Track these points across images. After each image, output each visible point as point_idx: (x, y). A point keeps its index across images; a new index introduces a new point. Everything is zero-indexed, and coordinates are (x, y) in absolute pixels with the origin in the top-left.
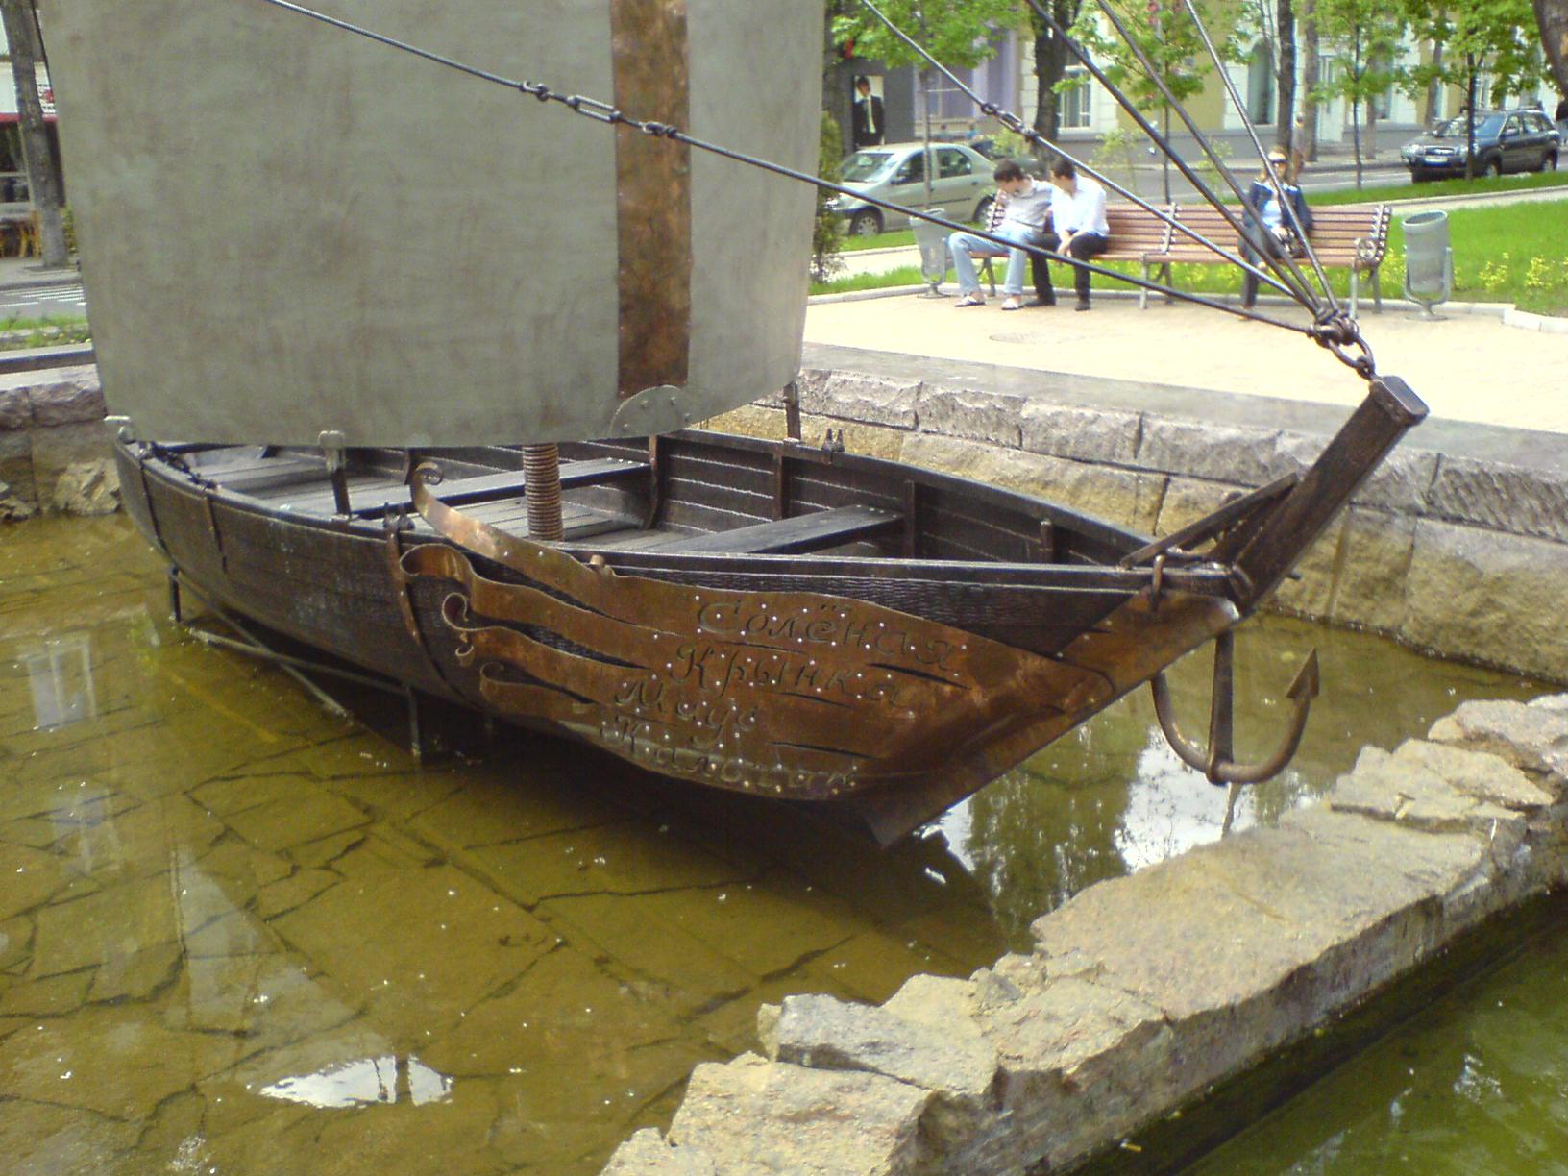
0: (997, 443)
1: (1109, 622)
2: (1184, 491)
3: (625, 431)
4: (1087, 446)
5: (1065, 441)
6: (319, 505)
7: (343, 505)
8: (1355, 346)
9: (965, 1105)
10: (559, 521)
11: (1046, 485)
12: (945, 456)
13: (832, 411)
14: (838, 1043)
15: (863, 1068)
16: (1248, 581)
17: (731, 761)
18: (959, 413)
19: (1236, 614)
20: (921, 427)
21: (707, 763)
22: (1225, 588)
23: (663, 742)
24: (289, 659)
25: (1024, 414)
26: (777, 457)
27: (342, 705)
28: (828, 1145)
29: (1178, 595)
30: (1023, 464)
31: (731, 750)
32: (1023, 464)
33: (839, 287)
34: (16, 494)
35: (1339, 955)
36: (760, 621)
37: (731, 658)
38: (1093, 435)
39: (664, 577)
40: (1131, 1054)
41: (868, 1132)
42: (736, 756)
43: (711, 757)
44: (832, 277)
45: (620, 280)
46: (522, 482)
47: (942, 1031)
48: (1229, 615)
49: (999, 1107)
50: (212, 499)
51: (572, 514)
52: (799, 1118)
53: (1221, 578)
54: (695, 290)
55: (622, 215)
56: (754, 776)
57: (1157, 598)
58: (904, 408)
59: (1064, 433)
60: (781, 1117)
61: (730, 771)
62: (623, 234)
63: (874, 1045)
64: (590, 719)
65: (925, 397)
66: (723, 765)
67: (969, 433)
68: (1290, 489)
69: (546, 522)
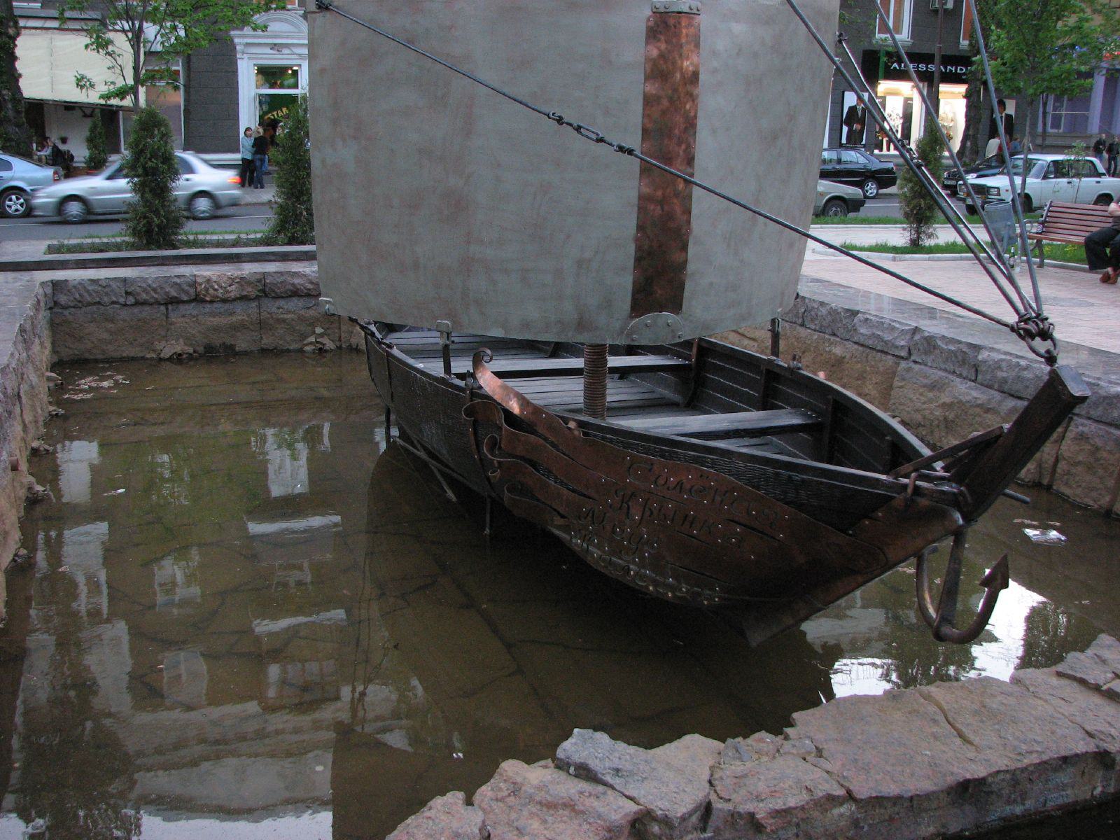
0: (960, 376)
1: (880, 514)
2: (1081, 428)
3: (633, 340)
4: (1019, 386)
5: (1005, 380)
6: (435, 367)
7: (447, 368)
8: (1049, 342)
9: (666, 821)
10: (604, 395)
11: (988, 410)
12: (925, 381)
13: (855, 339)
14: (594, 764)
15: (605, 784)
16: (969, 499)
17: (643, 571)
18: (937, 352)
19: (961, 522)
20: (913, 358)
21: (629, 570)
22: (955, 501)
23: (604, 552)
24: (433, 462)
25: (980, 357)
26: (763, 368)
27: (455, 495)
28: (562, 826)
29: (923, 502)
30: (974, 394)
31: (642, 565)
32: (974, 394)
33: (930, 250)
34: (328, 335)
35: (1017, 780)
36: (661, 481)
37: (646, 501)
38: (1023, 378)
39: (611, 441)
40: (816, 814)
41: (590, 824)
42: (644, 567)
43: (631, 567)
44: (928, 242)
45: (637, 240)
46: (582, 366)
47: (677, 772)
48: (956, 521)
49: (704, 830)
50: (389, 354)
51: (615, 392)
52: (551, 806)
53: (954, 494)
54: (692, 250)
55: (642, 198)
56: (656, 583)
57: (910, 503)
58: (903, 343)
59: (1004, 375)
60: (540, 803)
61: (643, 577)
62: (642, 210)
63: (618, 770)
64: (567, 529)
65: (917, 337)
66: (636, 571)
67: (943, 366)
68: (1000, 436)
69: (594, 393)
